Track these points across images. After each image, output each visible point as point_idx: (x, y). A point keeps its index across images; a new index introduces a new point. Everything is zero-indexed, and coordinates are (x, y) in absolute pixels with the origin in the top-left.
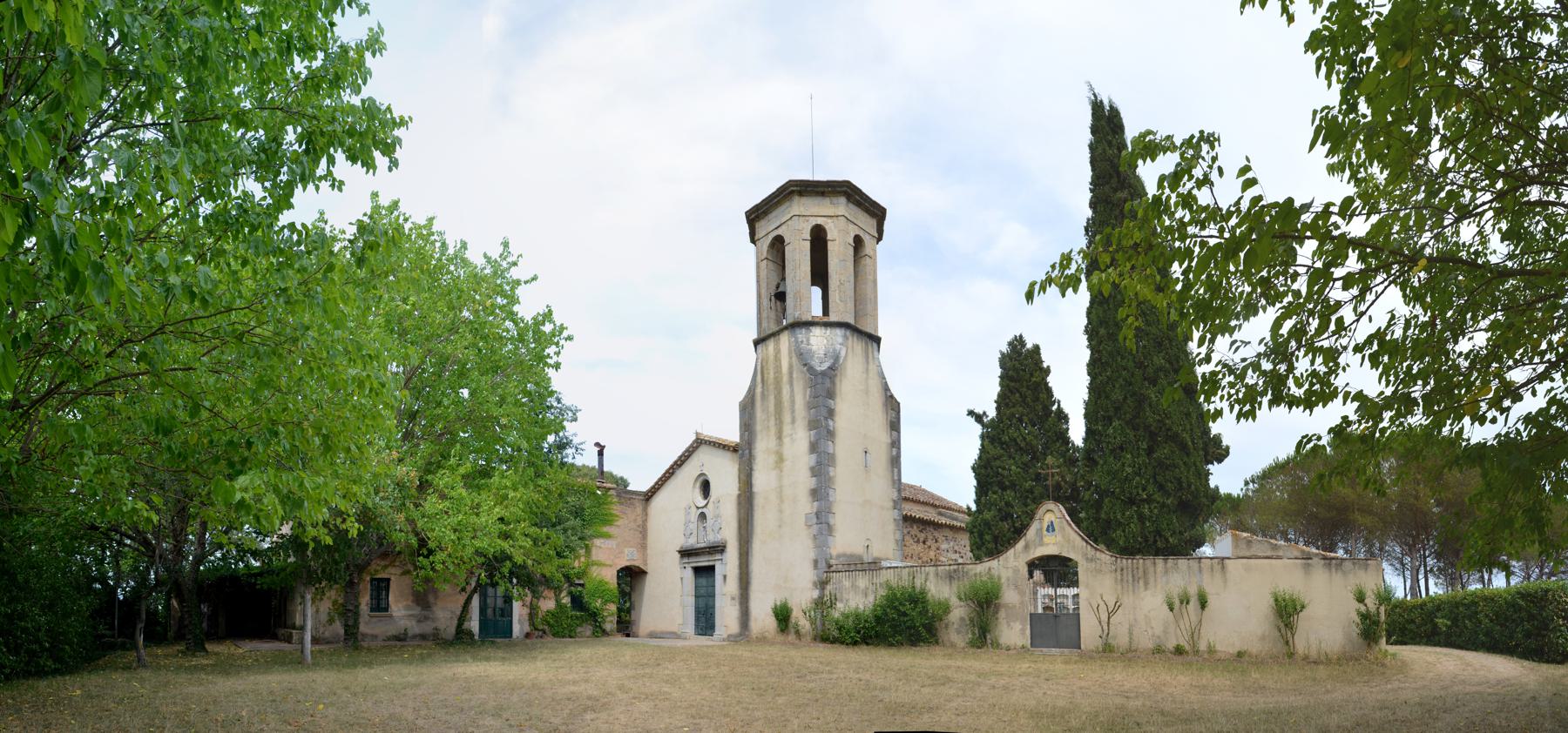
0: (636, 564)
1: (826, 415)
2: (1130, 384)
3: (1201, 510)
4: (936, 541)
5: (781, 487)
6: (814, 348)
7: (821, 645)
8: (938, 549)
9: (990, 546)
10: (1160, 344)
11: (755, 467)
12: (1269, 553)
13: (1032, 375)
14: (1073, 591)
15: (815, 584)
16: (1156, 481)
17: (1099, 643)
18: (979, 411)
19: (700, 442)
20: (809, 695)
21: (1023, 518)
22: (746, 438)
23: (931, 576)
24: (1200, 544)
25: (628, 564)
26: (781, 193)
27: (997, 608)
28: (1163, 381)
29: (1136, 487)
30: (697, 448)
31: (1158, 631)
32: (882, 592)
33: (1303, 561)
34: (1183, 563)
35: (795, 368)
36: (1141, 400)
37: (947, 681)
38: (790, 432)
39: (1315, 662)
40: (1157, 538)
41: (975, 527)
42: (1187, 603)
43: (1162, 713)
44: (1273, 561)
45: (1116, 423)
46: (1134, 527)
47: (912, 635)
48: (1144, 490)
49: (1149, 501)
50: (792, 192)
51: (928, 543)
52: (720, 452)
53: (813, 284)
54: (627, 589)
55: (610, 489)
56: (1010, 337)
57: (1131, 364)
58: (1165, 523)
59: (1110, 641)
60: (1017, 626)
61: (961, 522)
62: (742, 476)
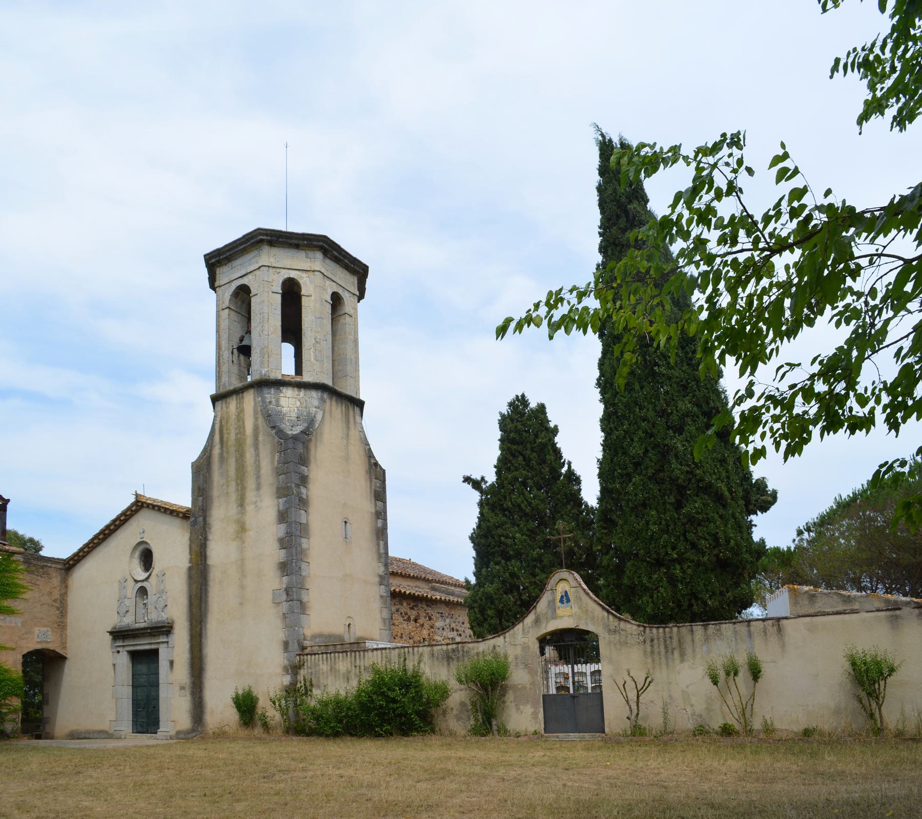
0: (51, 647)
1: (298, 482)
2: (652, 435)
3: (744, 568)
4: (430, 619)
5: (242, 560)
6: (285, 410)
7: (294, 738)
8: (432, 627)
9: (495, 621)
10: (685, 387)
11: (210, 537)
12: (840, 608)
13: (536, 436)
14: (593, 667)
15: (286, 669)
16: (686, 540)
17: (627, 725)
18: (476, 476)
19: (140, 505)
20: (276, 798)
21: (531, 589)
22: (200, 504)
23: (426, 658)
24: (747, 604)
25: (39, 647)
26: (248, 240)
27: (504, 690)
28: (691, 428)
29: (664, 547)
30: (136, 511)
31: (700, 707)
32: (367, 677)
33: (888, 613)
34: (727, 628)
35: (261, 429)
36: (665, 452)
37: (447, 774)
39: (913, 740)
40: (693, 601)
41: (474, 601)
42: (736, 674)
43: (712, 806)
44: (847, 616)
45: (636, 479)
46: (664, 591)
47: (403, 724)
48: (673, 549)
49: (681, 560)
50: (262, 241)
51: (421, 621)
52: (167, 518)
53: (284, 340)
54: (38, 678)
55: (13, 553)
56: (511, 397)
57: (651, 414)
58: (701, 584)
59: (640, 722)
60: (528, 710)
61: (459, 596)
62: (194, 547)
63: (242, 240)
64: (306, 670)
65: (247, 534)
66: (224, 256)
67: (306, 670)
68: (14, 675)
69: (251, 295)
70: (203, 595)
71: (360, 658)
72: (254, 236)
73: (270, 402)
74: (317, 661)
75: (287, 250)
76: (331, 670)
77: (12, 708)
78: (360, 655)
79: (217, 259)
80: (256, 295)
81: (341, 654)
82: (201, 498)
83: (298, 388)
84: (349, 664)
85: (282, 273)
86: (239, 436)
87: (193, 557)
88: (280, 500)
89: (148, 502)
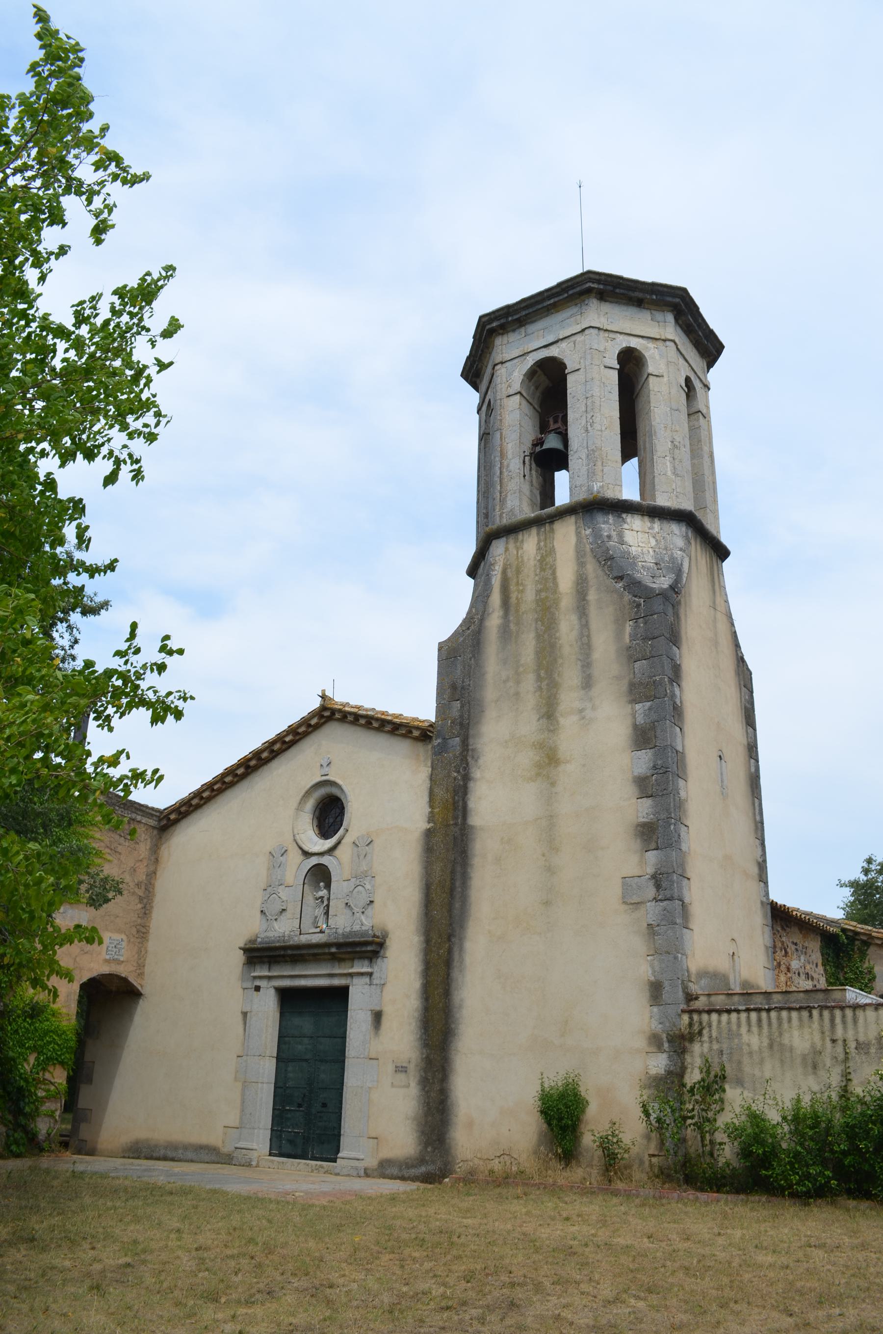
6: (634, 550)
11: (476, 774)
15: (655, 1041)
25: (106, 969)
30: (317, 727)
38: (577, 705)
50: (589, 291)
52: (382, 741)
62: (440, 792)
63: (554, 291)
64: (706, 1045)
65: (561, 768)
66: (515, 317)
67: (706, 1045)
68: (64, 1023)
69: (566, 371)
70: (458, 884)
71: (844, 1022)
72: (578, 283)
73: (609, 537)
74: (734, 1027)
75: (624, 308)
76: (771, 1046)
77: (52, 1088)
78: (844, 1016)
79: (503, 321)
80: (578, 370)
81: (794, 1014)
82: (457, 704)
83: (650, 516)
84: (817, 1037)
85: (618, 340)
86: (543, 595)
87: (436, 810)
88: (638, 707)
89: (347, 709)
